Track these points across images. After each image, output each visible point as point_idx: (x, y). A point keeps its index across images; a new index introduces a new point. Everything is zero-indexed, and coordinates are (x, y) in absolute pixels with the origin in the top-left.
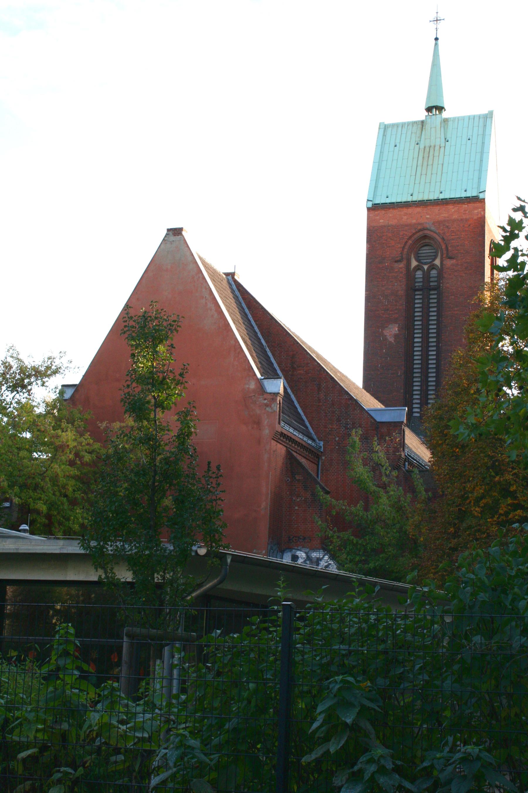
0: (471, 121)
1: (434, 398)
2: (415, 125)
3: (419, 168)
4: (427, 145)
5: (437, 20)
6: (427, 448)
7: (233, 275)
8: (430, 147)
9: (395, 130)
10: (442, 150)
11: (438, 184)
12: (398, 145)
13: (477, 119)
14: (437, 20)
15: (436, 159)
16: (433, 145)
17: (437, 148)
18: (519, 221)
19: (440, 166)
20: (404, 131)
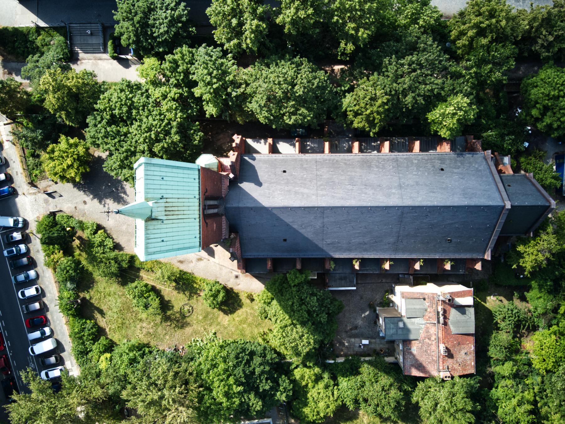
0: (149, 177)
1: (85, 404)
2: (148, 228)
3: (180, 217)
4: (164, 213)
5: (108, 212)
6: (241, 300)
7: (230, 258)
8: (166, 211)
9: (150, 245)
10: (168, 200)
11: (190, 200)
12: (162, 239)
13: (149, 173)
14: (108, 212)
15: (174, 204)
16: (163, 209)
17: (167, 205)
18: (465, 310)
19: (179, 200)
20: (152, 236)
